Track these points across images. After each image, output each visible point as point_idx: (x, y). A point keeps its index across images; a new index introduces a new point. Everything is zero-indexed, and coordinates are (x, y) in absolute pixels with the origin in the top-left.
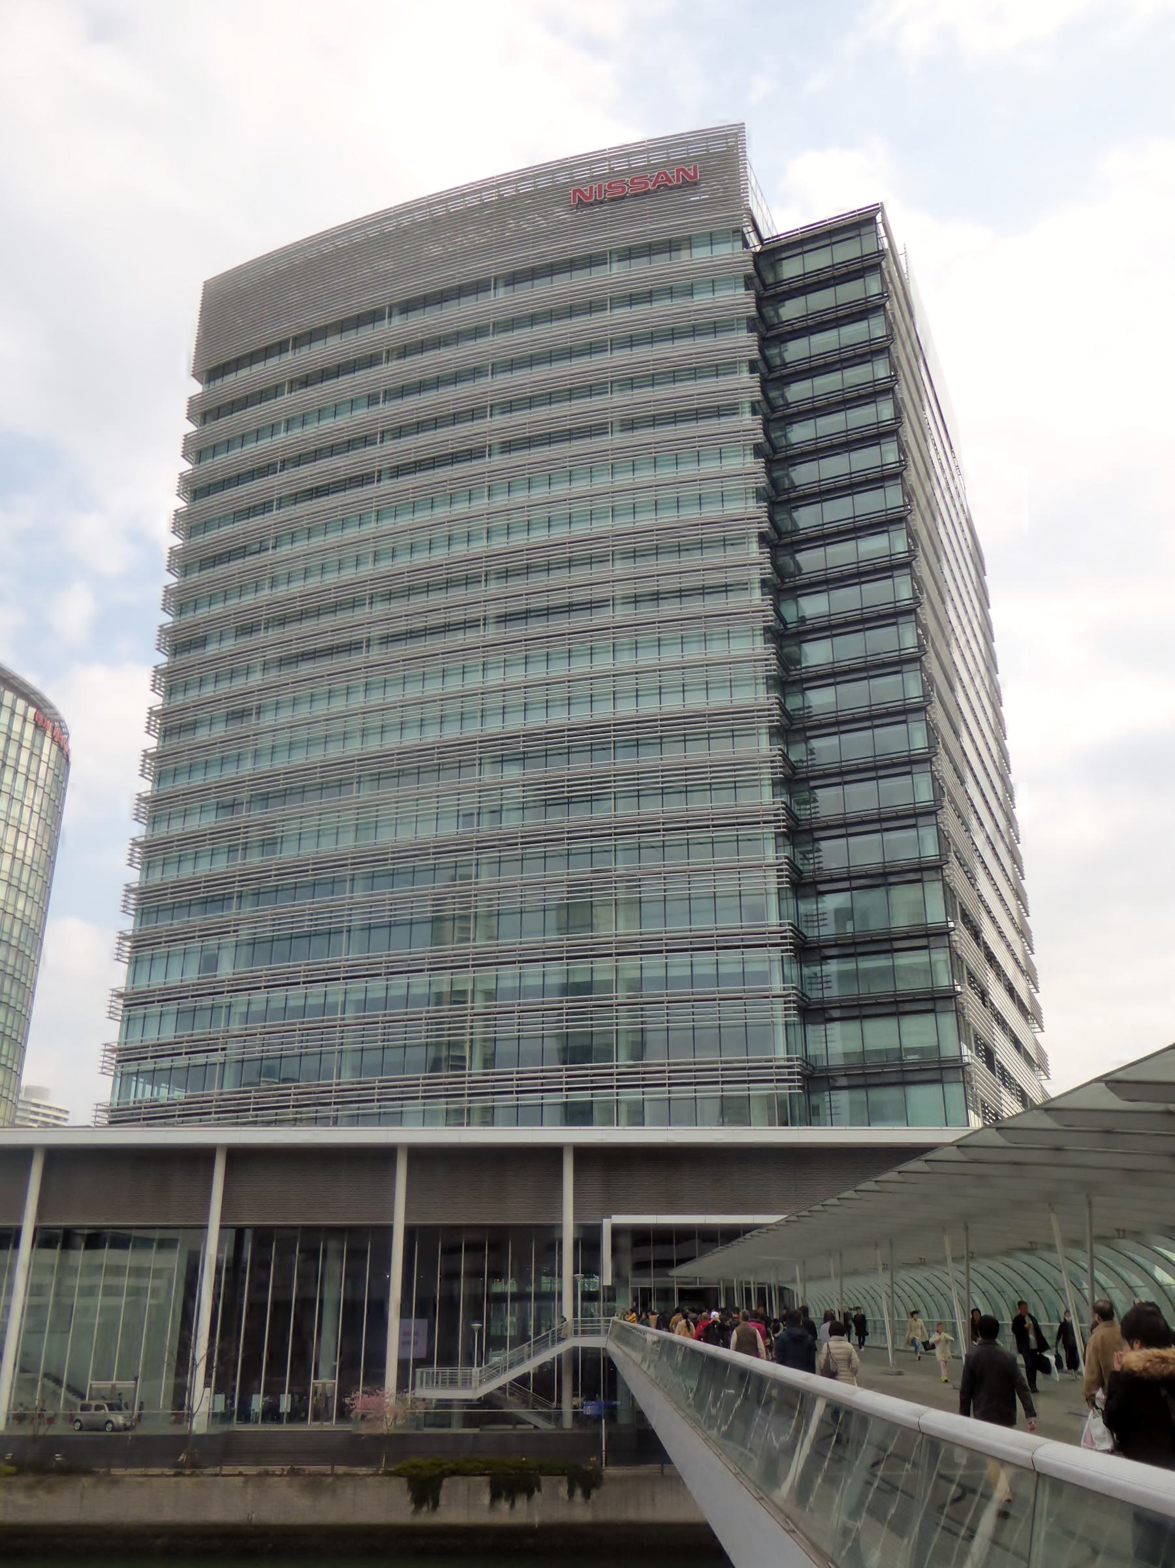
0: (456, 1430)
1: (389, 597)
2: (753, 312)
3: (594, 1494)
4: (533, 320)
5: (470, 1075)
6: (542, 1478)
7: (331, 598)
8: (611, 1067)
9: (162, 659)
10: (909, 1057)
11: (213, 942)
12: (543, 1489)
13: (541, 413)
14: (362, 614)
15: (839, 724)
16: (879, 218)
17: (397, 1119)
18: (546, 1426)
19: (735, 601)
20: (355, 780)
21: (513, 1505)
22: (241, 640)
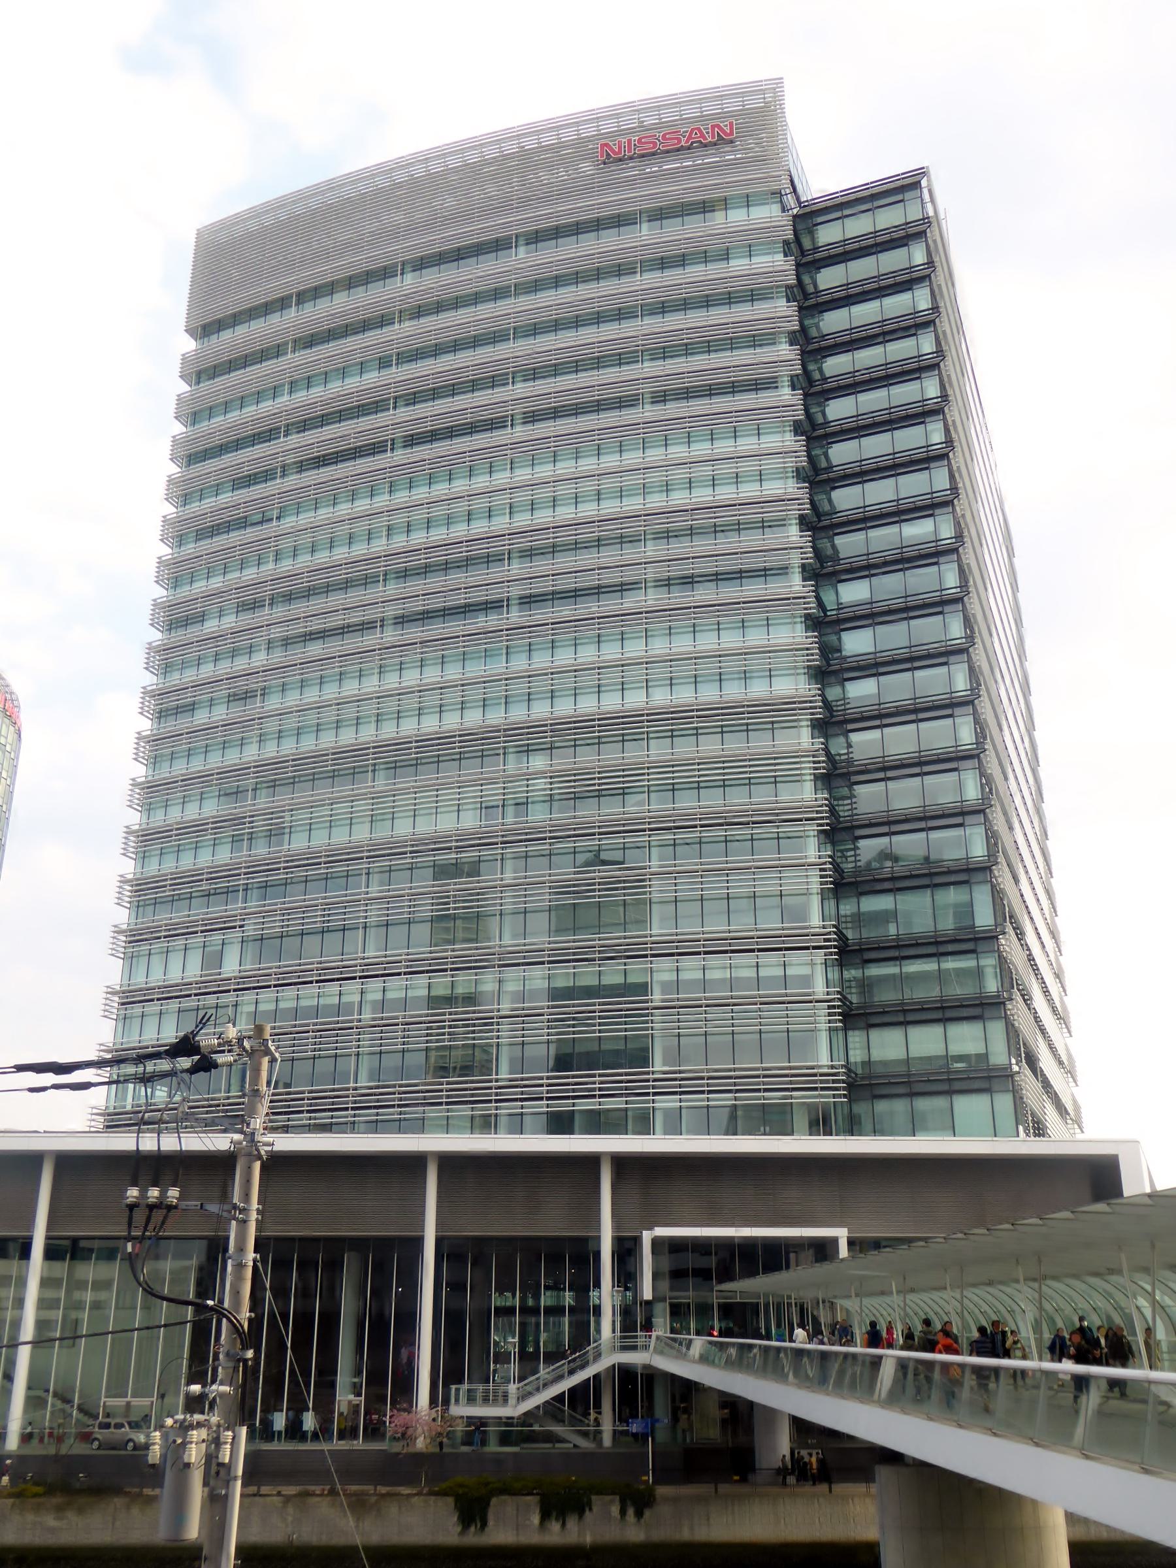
0: (493, 1448)
1: (289, 597)
2: (792, 281)
3: (647, 1513)
4: (557, 282)
5: (497, 1081)
6: (594, 1498)
7: (342, 575)
8: (648, 1073)
9: (156, 636)
10: (956, 1065)
11: (217, 937)
12: (595, 1509)
13: (443, 405)
14: (376, 592)
15: (880, 716)
16: (924, 183)
17: (420, 1126)
18: (585, 1444)
19: (776, 587)
20: (370, 768)
21: (564, 1525)
22: (242, 616)
